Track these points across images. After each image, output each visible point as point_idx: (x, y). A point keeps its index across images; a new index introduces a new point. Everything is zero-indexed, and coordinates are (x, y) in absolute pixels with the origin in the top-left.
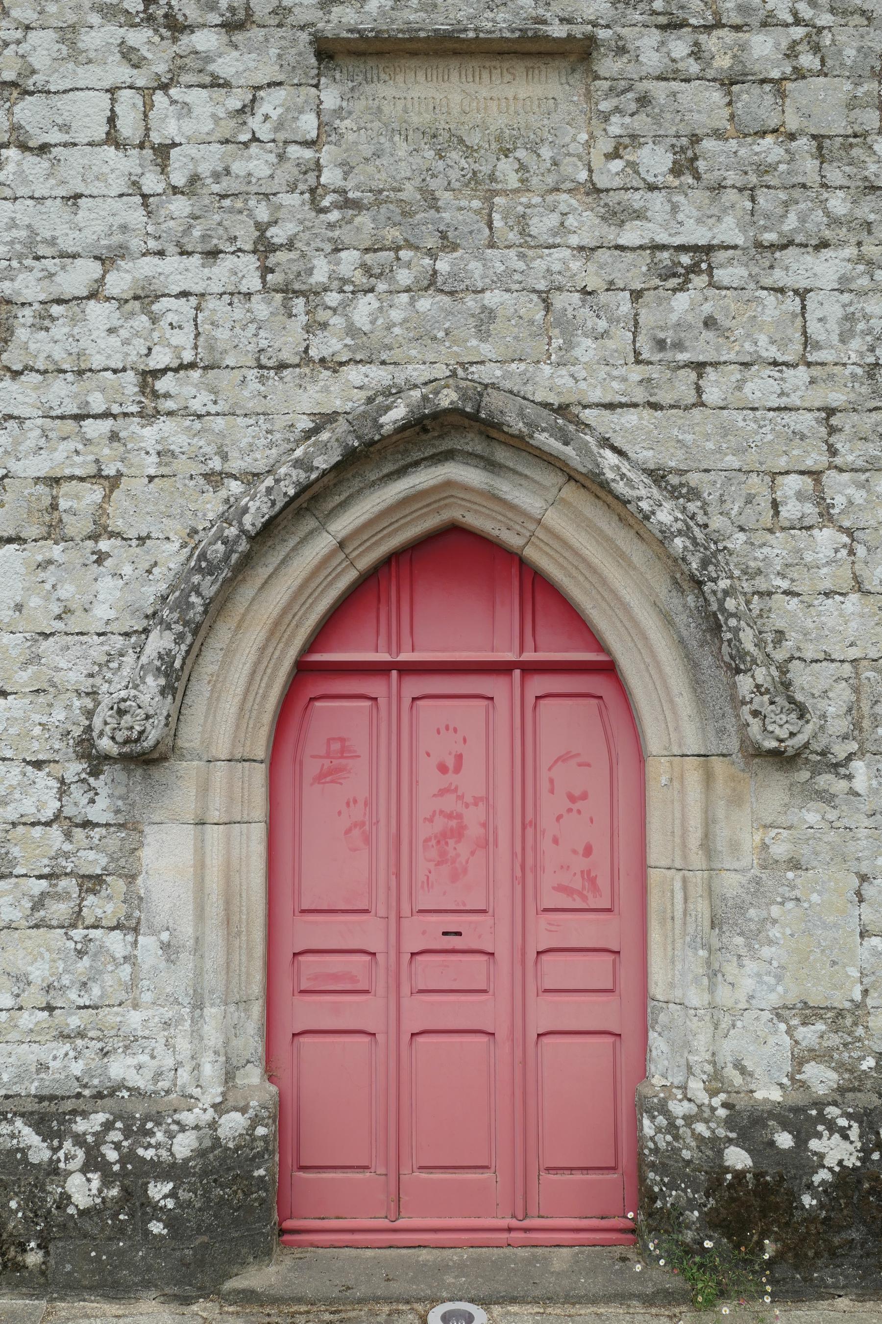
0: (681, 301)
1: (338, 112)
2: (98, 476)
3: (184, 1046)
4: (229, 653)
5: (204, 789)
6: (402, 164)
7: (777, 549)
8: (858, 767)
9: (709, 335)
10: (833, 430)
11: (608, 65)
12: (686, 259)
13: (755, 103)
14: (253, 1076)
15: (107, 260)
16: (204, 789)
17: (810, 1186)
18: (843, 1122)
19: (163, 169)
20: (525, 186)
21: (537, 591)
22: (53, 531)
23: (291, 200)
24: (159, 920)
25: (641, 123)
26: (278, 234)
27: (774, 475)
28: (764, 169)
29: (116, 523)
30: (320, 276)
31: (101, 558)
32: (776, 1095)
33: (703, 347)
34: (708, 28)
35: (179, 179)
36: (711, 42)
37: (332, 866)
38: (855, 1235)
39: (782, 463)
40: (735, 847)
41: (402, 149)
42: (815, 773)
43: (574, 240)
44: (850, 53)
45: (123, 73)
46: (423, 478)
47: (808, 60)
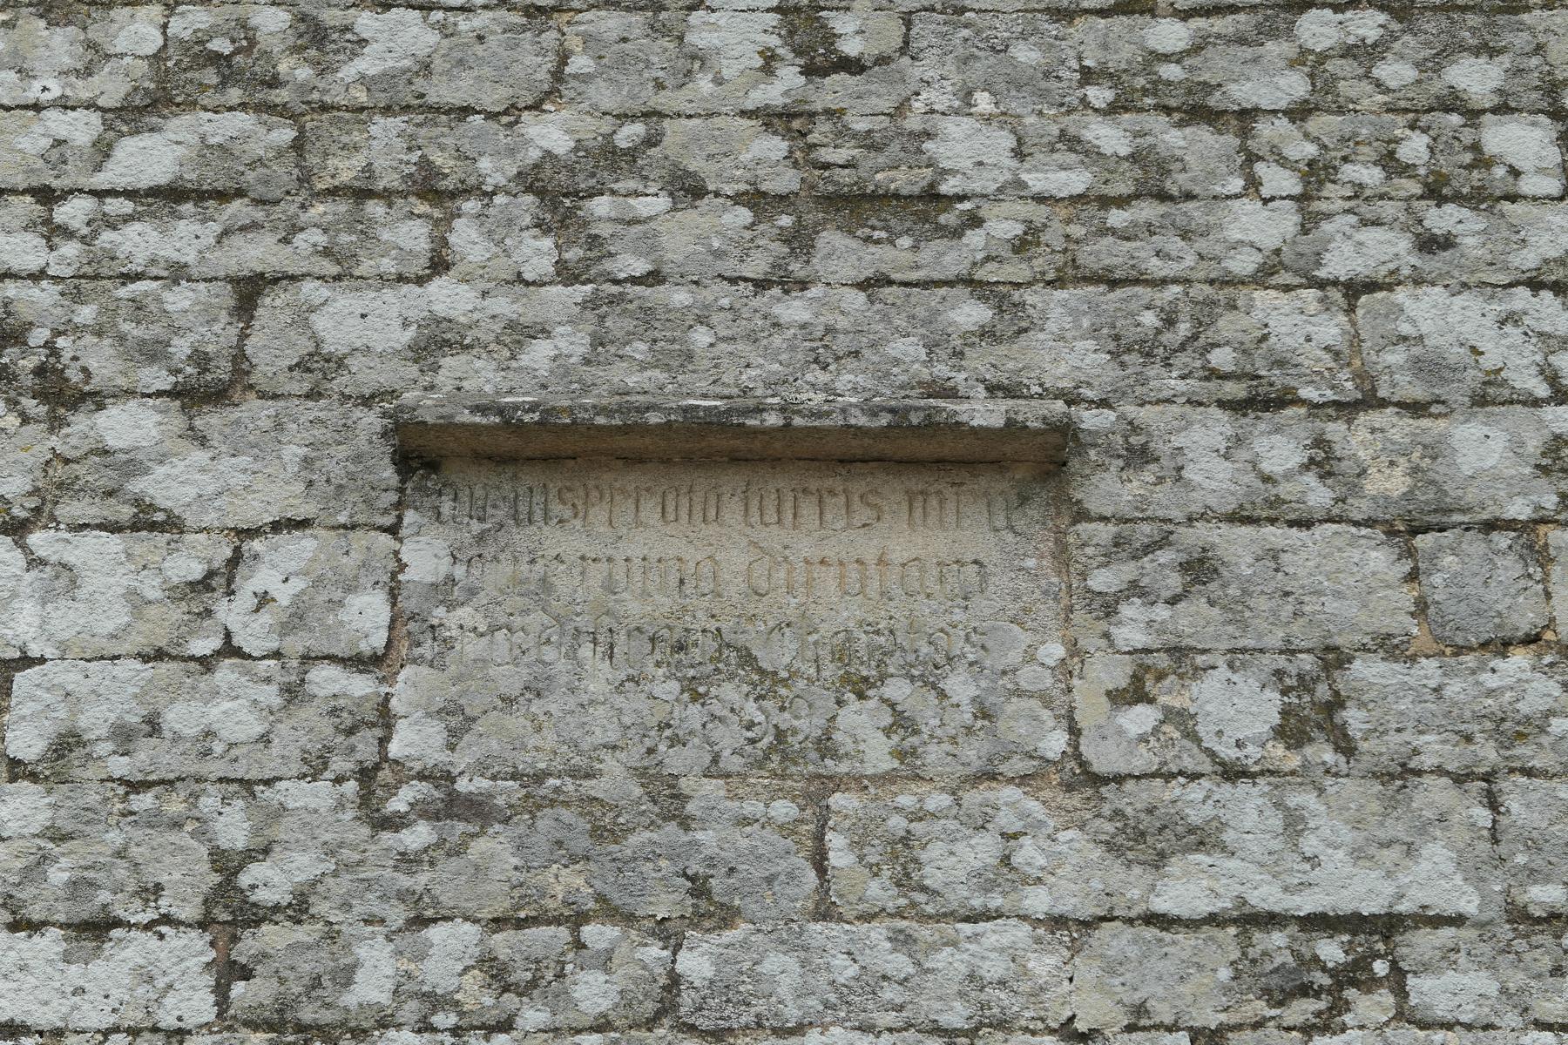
1: (443, 591)
6: (599, 712)
11: (1108, 489)
12: (1331, 950)
25: (1195, 619)
26: (266, 882)
34: (1346, 409)
36: (1354, 440)
41: (599, 676)
43: (1038, 901)
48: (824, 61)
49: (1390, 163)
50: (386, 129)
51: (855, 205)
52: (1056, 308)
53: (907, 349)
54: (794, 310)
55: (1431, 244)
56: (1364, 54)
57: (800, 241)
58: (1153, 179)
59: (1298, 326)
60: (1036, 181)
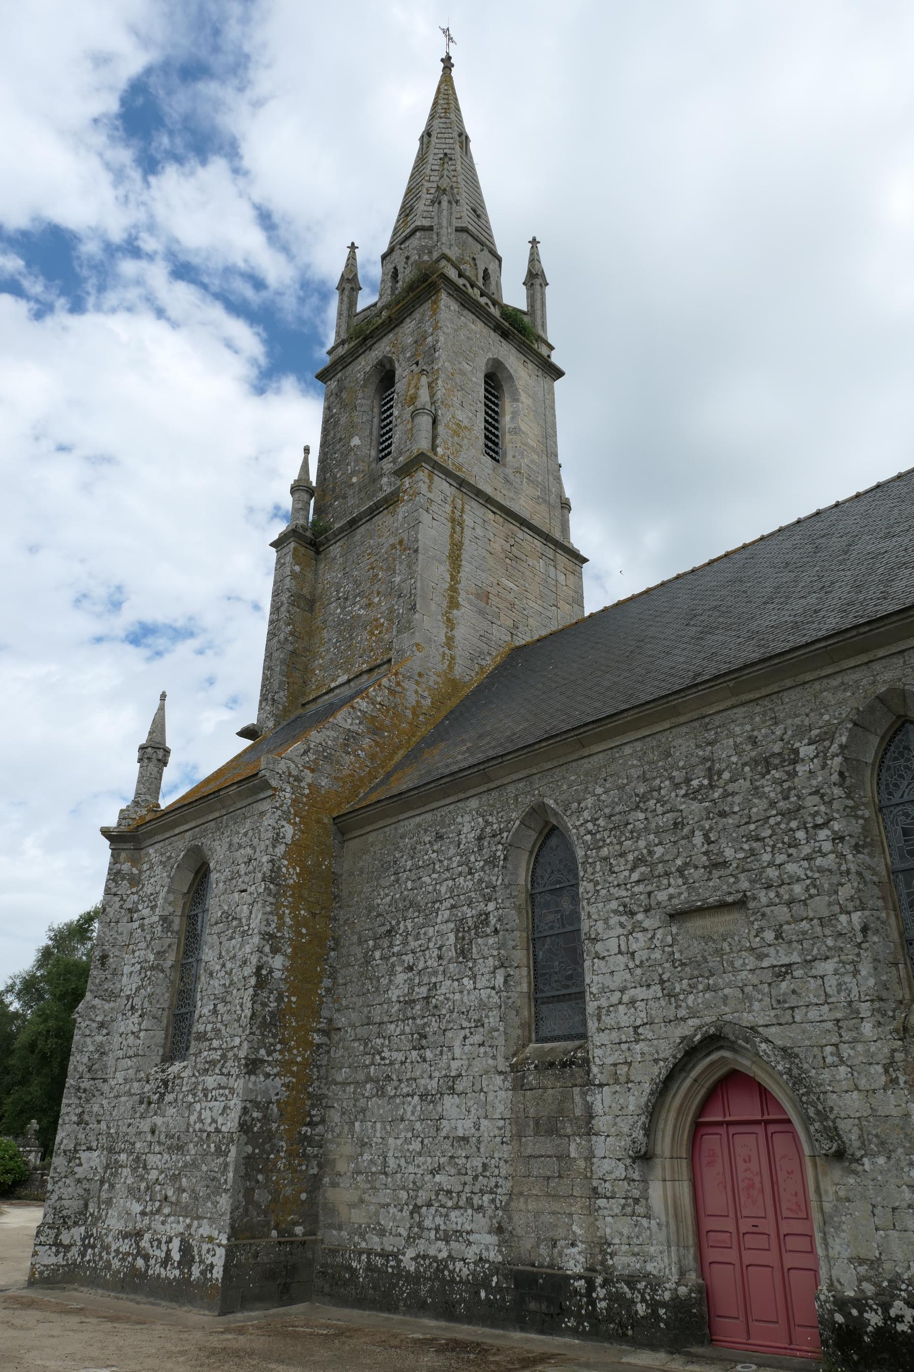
0: (784, 985)
1: (677, 934)
2: (626, 1063)
3: (666, 1259)
4: (666, 1121)
5: (664, 1169)
6: (696, 948)
7: (826, 1075)
8: (865, 1160)
9: (794, 996)
10: (840, 1028)
11: (752, 905)
12: (783, 970)
13: (797, 909)
14: (692, 1276)
15: (622, 991)
16: (664, 1169)
17: (866, 1333)
18: (875, 1307)
19: (633, 959)
20: (732, 951)
21: (764, 1094)
22: (617, 1082)
23: (667, 965)
24: (656, 1214)
25: (763, 923)
26: (665, 977)
27: (822, 1047)
28: (804, 933)
29: (632, 1078)
30: (677, 990)
31: (629, 1089)
32: (852, 1294)
33: (793, 1001)
34: (780, 886)
35: (638, 963)
36: (782, 891)
37: (715, 1199)
38: (886, 1356)
39: (824, 1042)
40: (827, 1192)
41: (696, 943)
42: (850, 1163)
43: (748, 968)
44: (826, 886)
45: (620, 931)
46: (714, 1056)
47: (813, 891)
48: (710, 843)
49: (783, 843)
50: (660, 865)
51: (716, 865)
52: (742, 877)
53: (725, 887)
54: (711, 884)
55: (789, 855)
56: (778, 824)
57: (710, 872)
58: (752, 852)
59: (772, 873)
60: (738, 856)
